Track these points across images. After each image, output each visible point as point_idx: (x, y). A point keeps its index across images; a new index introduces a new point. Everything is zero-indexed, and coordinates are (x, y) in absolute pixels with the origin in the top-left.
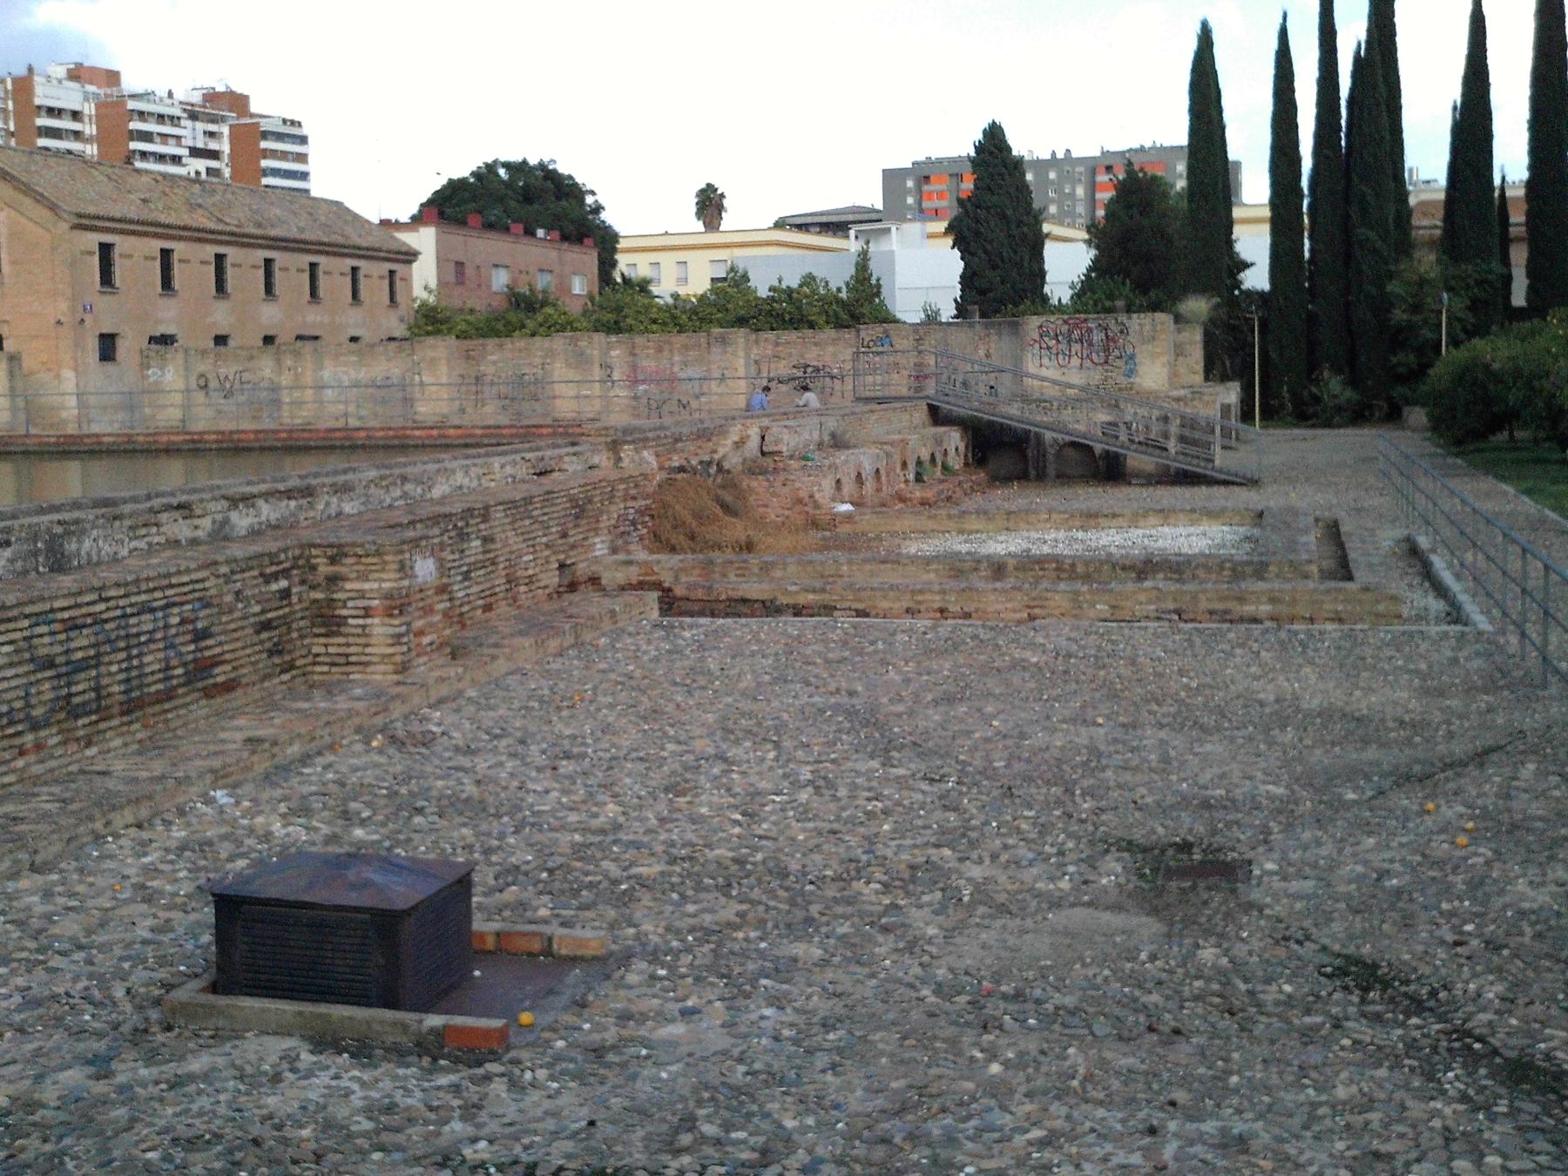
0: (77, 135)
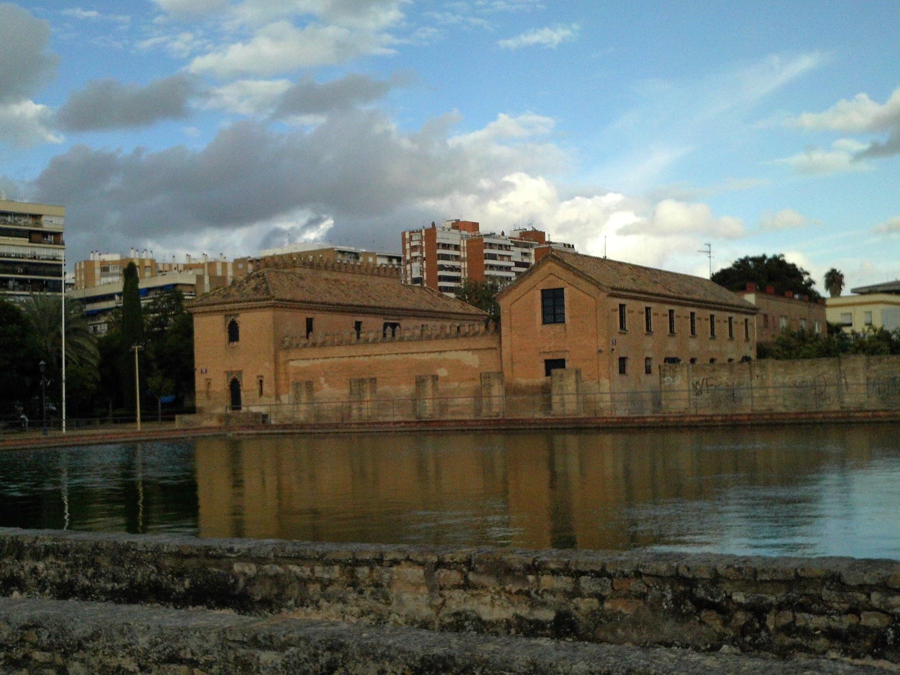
0: (457, 258)
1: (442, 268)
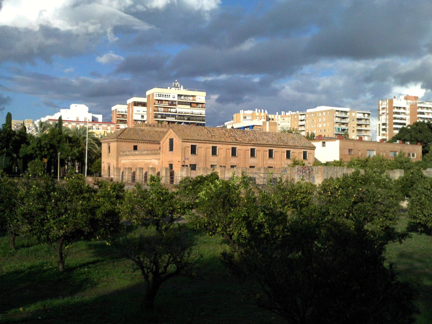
1: (395, 118)
